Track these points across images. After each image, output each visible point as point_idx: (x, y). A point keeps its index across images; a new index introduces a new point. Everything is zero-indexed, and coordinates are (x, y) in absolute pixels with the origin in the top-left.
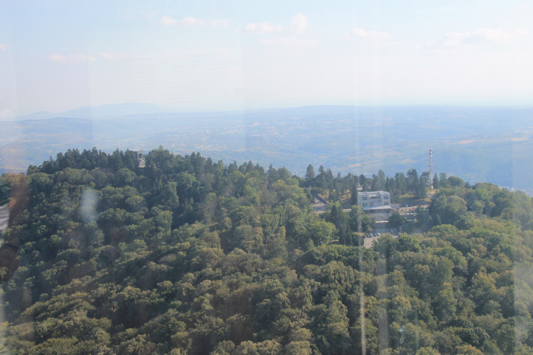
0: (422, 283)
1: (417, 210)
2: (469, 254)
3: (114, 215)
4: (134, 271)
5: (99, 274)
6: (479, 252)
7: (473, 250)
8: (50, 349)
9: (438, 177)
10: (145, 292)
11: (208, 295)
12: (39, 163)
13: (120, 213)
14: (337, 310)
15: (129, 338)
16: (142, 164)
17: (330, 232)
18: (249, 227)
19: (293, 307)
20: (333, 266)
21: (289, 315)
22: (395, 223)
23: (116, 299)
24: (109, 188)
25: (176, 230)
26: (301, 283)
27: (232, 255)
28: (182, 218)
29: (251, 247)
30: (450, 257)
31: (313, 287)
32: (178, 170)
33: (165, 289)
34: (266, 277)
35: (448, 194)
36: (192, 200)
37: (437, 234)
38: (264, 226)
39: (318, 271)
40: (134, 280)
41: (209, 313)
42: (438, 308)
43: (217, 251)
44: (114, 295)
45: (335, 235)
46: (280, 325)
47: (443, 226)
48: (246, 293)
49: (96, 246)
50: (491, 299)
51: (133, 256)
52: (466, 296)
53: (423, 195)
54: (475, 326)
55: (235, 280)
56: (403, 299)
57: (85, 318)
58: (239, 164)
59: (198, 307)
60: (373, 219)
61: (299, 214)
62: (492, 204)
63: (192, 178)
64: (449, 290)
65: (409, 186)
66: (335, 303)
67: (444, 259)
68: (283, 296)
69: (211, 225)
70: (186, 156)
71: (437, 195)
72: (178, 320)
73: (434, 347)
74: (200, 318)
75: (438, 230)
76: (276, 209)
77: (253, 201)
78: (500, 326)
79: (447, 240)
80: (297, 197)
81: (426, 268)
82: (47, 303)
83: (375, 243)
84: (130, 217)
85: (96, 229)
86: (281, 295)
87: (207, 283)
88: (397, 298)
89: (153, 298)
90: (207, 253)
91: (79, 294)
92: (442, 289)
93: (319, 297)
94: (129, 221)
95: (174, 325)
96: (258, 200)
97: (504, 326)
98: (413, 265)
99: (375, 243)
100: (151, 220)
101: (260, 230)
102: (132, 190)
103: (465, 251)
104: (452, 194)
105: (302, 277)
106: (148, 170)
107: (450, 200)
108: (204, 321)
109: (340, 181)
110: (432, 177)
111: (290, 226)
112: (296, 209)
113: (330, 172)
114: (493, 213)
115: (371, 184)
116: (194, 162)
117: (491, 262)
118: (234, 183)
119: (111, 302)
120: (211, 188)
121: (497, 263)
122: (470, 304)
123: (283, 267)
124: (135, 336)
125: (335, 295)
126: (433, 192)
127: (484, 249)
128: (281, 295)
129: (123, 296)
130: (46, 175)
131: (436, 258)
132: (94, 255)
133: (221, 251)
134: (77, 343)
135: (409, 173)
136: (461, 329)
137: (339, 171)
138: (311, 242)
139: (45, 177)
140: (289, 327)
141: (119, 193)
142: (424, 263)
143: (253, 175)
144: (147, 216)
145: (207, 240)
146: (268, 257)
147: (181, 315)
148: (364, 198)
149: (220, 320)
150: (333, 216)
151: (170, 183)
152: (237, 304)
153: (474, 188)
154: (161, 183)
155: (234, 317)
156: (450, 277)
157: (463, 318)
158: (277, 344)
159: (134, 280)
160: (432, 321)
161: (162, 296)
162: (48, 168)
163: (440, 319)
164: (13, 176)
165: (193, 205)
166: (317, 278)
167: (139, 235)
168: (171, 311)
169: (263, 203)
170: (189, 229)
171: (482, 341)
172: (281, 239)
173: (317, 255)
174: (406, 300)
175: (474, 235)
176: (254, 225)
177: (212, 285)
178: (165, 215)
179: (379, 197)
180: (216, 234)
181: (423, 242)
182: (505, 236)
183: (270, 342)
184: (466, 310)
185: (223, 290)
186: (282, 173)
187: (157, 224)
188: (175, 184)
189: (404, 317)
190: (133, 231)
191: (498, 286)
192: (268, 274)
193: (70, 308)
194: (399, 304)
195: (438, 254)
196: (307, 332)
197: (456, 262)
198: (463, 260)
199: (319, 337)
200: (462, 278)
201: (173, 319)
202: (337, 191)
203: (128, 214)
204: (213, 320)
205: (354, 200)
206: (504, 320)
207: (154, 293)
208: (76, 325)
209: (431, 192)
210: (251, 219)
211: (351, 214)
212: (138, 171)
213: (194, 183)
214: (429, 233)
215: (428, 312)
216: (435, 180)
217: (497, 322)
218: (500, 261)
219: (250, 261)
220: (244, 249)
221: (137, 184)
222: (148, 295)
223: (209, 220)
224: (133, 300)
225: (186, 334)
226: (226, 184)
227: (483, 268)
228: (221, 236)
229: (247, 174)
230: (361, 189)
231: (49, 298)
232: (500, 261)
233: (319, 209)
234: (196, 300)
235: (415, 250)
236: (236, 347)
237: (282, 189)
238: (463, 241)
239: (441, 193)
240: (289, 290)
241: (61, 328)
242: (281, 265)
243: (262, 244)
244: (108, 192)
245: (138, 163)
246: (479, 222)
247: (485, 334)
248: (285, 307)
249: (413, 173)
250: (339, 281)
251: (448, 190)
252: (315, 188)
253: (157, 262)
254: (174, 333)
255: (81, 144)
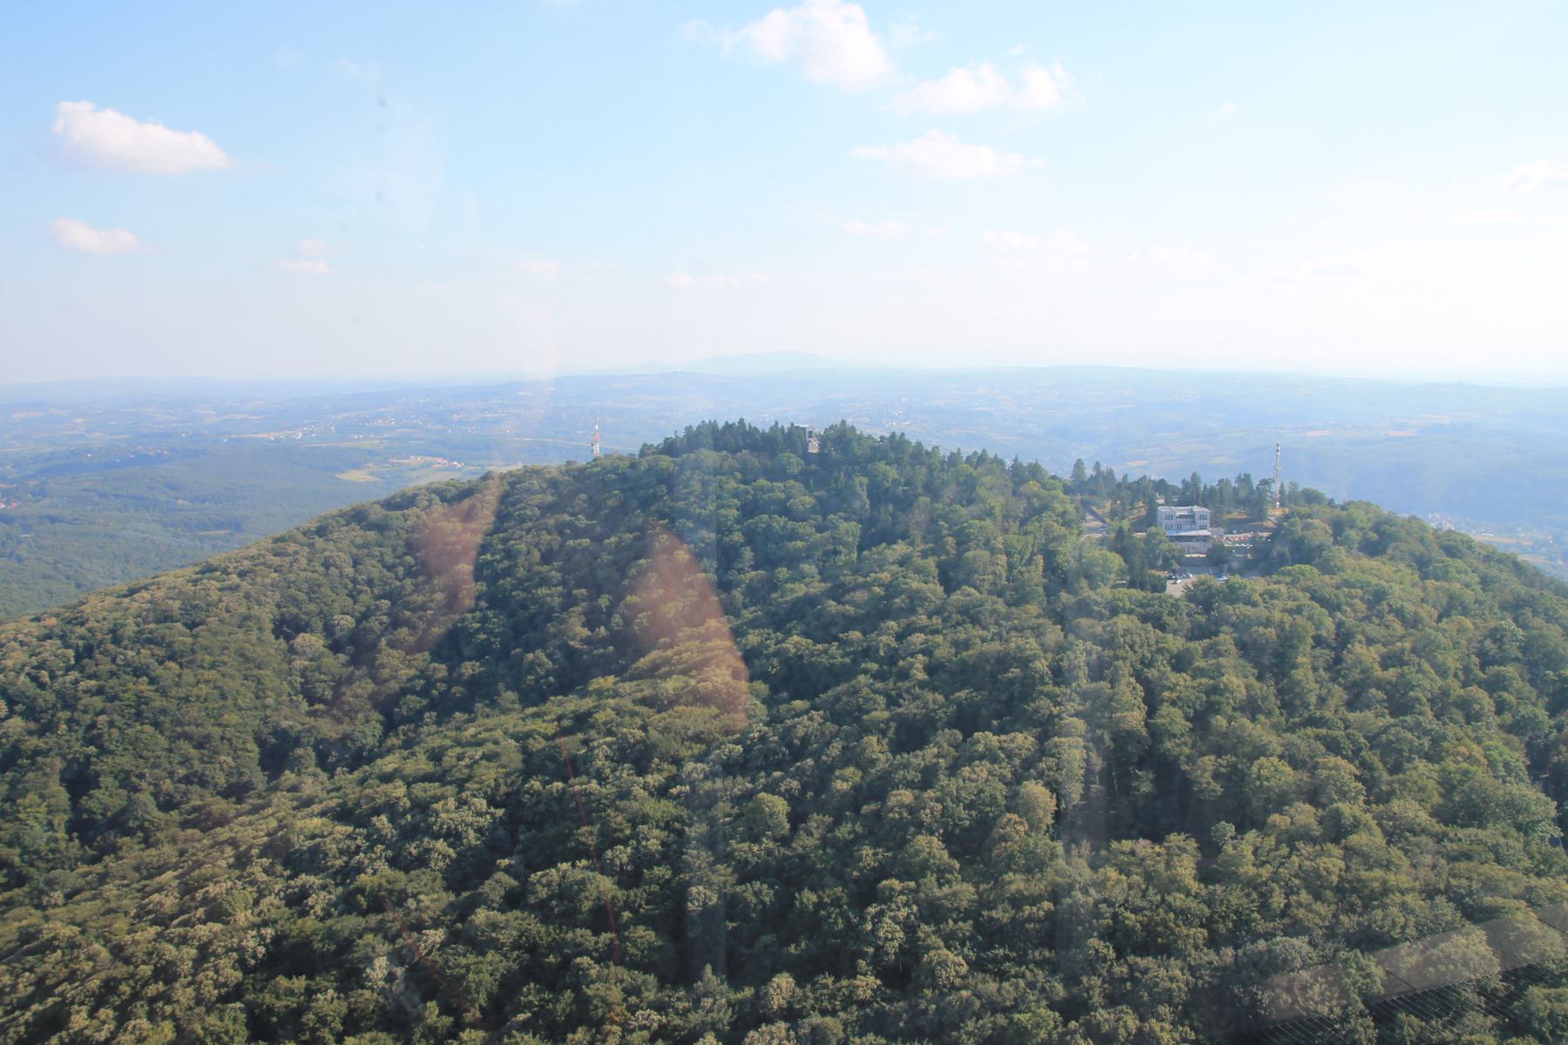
0: (1273, 661)
1: (1253, 540)
2: (1339, 614)
3: (769, 526)
4: (802, 611)
5: (747, 615)
6: (1355, 611)
7: (1345, 607)
8: (679, 722)
9: (1287, 490)
10: (819, 647)
11: (920, 657)
12: (657, 441)
13: (779, 522)
14: (1128, 691)
15: (798, 715)
16: (814, 447)
17: (1116, 568)
18: (986, 554)
19: (1057, 684)
20: (1123, 622)
21: (1052, 697)
22: (1217, 559)
23: (775, 654)
24: (762, 482)
25: (866, 553)
26: (1070, 647)
27: (957, 597)
28: (875, 536)
29: (987, 585)
30: (1310, 618)
31: (1089, 653)
32: (871, 459)
33: (851, 643)
34: (1013, 633)
35: (1302, 517)
36: (891, 507)
37: (1288, 579)
38: (1009, 554)
39: (1099, 630)
40: (801, 627)
41: (922, 685)
42: (1290, 700)
43: (935, 589)
44: (772, 649)
45: (1121, 573)
46: (1036, 711)
47: (1297, 567)
48: (983, 656)
49: (740, 571)
50: (1370, 686)
51: (800, 590)
52: (1334, 680)
53: (1261, 516)
54: (1347, 727)
55: (963, 636)
56: (1234, 679)
57: (729, 679)
58: (966, 452)
59: (904, 675)
60: (1182, 551)
61: (1065, 537)
62: (1374, 536)
63: (892, 473)
64: (1306, 670)
65: (1240, 500)
66: (1123, 681)
67: (1300, 620)
68: (1041, 665)
69: (922, 547)
70: (882, 438)
71: (1286, 518)
72: (875, 692)
73: (1281, 757)
74: (908, 692)
75: (1289, 573)
76: (1029, 527)
77: (989, 514)
78: (1386, 730)
79: (1303, 590)
80: (1060, 509)
81: (1271, 632)
82: (669, 653)
83: (1187, 588)
84: (793, 530)
85: (743, 545)
86: (1038, 664)
87: (917, 639)
88: (1224, 679)
89: (832, 657)
90: (918, 591)
91: (718, 642)
92: (1295, 666)
93: (1099, 671)
94: (793, 536)
95: (867, 700)
96: (997, 511)
97: (1393, 730)
98: (1250, 626)
99: (1187, 588)
100: (826, 534)
101: (1002, 559)
102: (798, 486)
103: (1332, 607)
104: (1309, 516)
105: (1071, 637)
106: (822, 458)
107: (1307, 527)
108: (915, 698)
109: (1129, 487)
110: (1275, 488)
111: (1049, 556)
112: (1058, 529)
113: (1111, 473)
114: (1373, 548)
115: (1190, 494)
116: (895, 448)
117: (1372, 630)
118: (958, 484)
119: (768, 657)
120: (920, 490)
121: (1383, 631)
122: (1339, 694)
123: (1041, 620)
124: (807, 712)
125: (1125, 669)
126: (1278, 513)
127: (1362, 607)
128: (1038, 664)
129: (787, 651)
130: (668, 458)
131: (1287, 618)
132: (738, 585)
133: (940, 589)
134: (717, 716)
135: (1239, 479)
136: (1323, 731)
137: (1130, 469)
138: (1084, 583)
139: (666, 462)
140: (1051, 714)
141: (778, 490)
142: (1267, 623)
143: (990, 472)
144: (820, 530)
145: (918, 571)
146: (1016, 603)
147: (879, 685)
148: (1170, 517)
149: (940, 698)
150: (1120, 544)
151: (857, 480)
152: (964, 674)
153: (1343, 508)
154: (842, 478)
155: (962, 694)
156: (1308, 649)
157: (1328, 714)
158: (1031, 739)
159: (801, 627)
160: (1279, 717)
161: (846, 654)
162: (670, 448)
163: (1291, 715)
164: (621, 458)
165: (894, 516)
166: (1097, 640)
167: (808, 557)
168: (862, 678)
169: (1006, 517)
170: (888, 552)
171: (1356, 752)
172: (1035, 574)
173: (1096, 603)
174: (1237, 680)
175: (1347, 583)
176: (993, 551)
177: (926, 641)
178: (849, 529)
179: (1192, 516)
180: (931, 563)
181: (1266, 592)
182: (1396, 587)
183: (1020, 736)
184: (1332, 703)
185: (944, 651)
186: (1035, 470)
187: (835, 540)
188: (865, 480)
189: (1234, 709)
190: (800, 550)
191: (1385, 667)
192: (1015, 629)
193: (705, 663)
194: (1226, 689)
195: (1290, 612)
196: (1080, 725)
197: (1318, 626)
198: (1329, 623)
199: (1099, 732)
200: (1327, 651)
201: (865, 690)
202: (1123, 504)
203: (790, 524)
204: (930, 696)
205: (1150, 519)
206: (1393, 721)
207: (834, 648)
208: (717, 691)
209: (1275, 513)
210: (987, 543)
211: (1147, 541)
212: (805, 456)
213: (894, 481)
214: (1275, 577)
215: (1273, 702)
216: (1282, 491)
217: (1381, 722)
218: (1387, 627)
219: (988, 606)
220: (976, 588)
221: (804, 477)
222: (825, 652)
223: (918, 540)
224: (802, 657)
225: (886, 714)
226: (945, 484)
227: (1360, 637)
228: (939, 565)
229: (980, 469)
230: (1161, 501)
231: (671, 646)
232: (1387, 627)
233: (1092, 530)
234: (901, 663)
235: (1254, 605)
236: (964, 740)
237: (1036, 495)
238: (1328, 592)
239: (1292, 514)
240: (1050, 656)
241: (694, 692)
242: (1037, 617)
243: (1004, 582)
244: (762, 488)
245: (806, 445)
246: (1352, 564)
247: (1362, 740)
248: (1044, 684)
249: (1245, 480)
250: (1132, 647)
251: (1304, 510)
252: (1086, 497)
253: (839, 602)
254: (868, 712)
255: (725, 415)
